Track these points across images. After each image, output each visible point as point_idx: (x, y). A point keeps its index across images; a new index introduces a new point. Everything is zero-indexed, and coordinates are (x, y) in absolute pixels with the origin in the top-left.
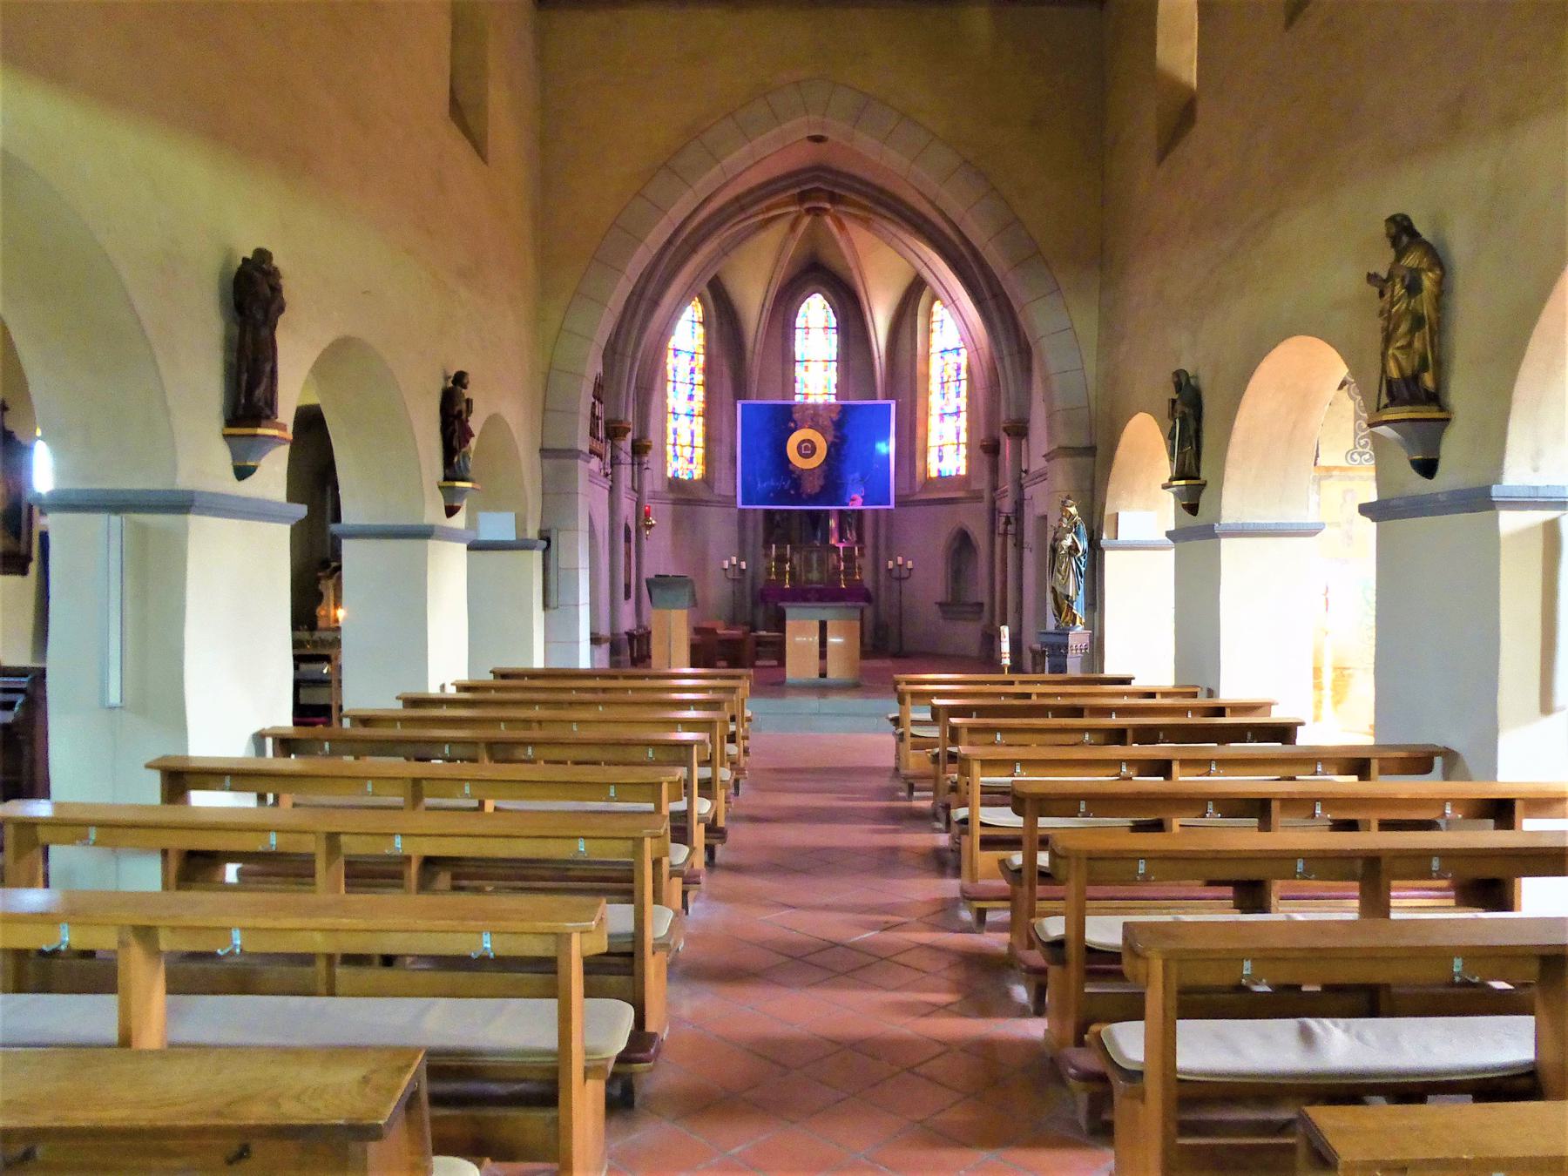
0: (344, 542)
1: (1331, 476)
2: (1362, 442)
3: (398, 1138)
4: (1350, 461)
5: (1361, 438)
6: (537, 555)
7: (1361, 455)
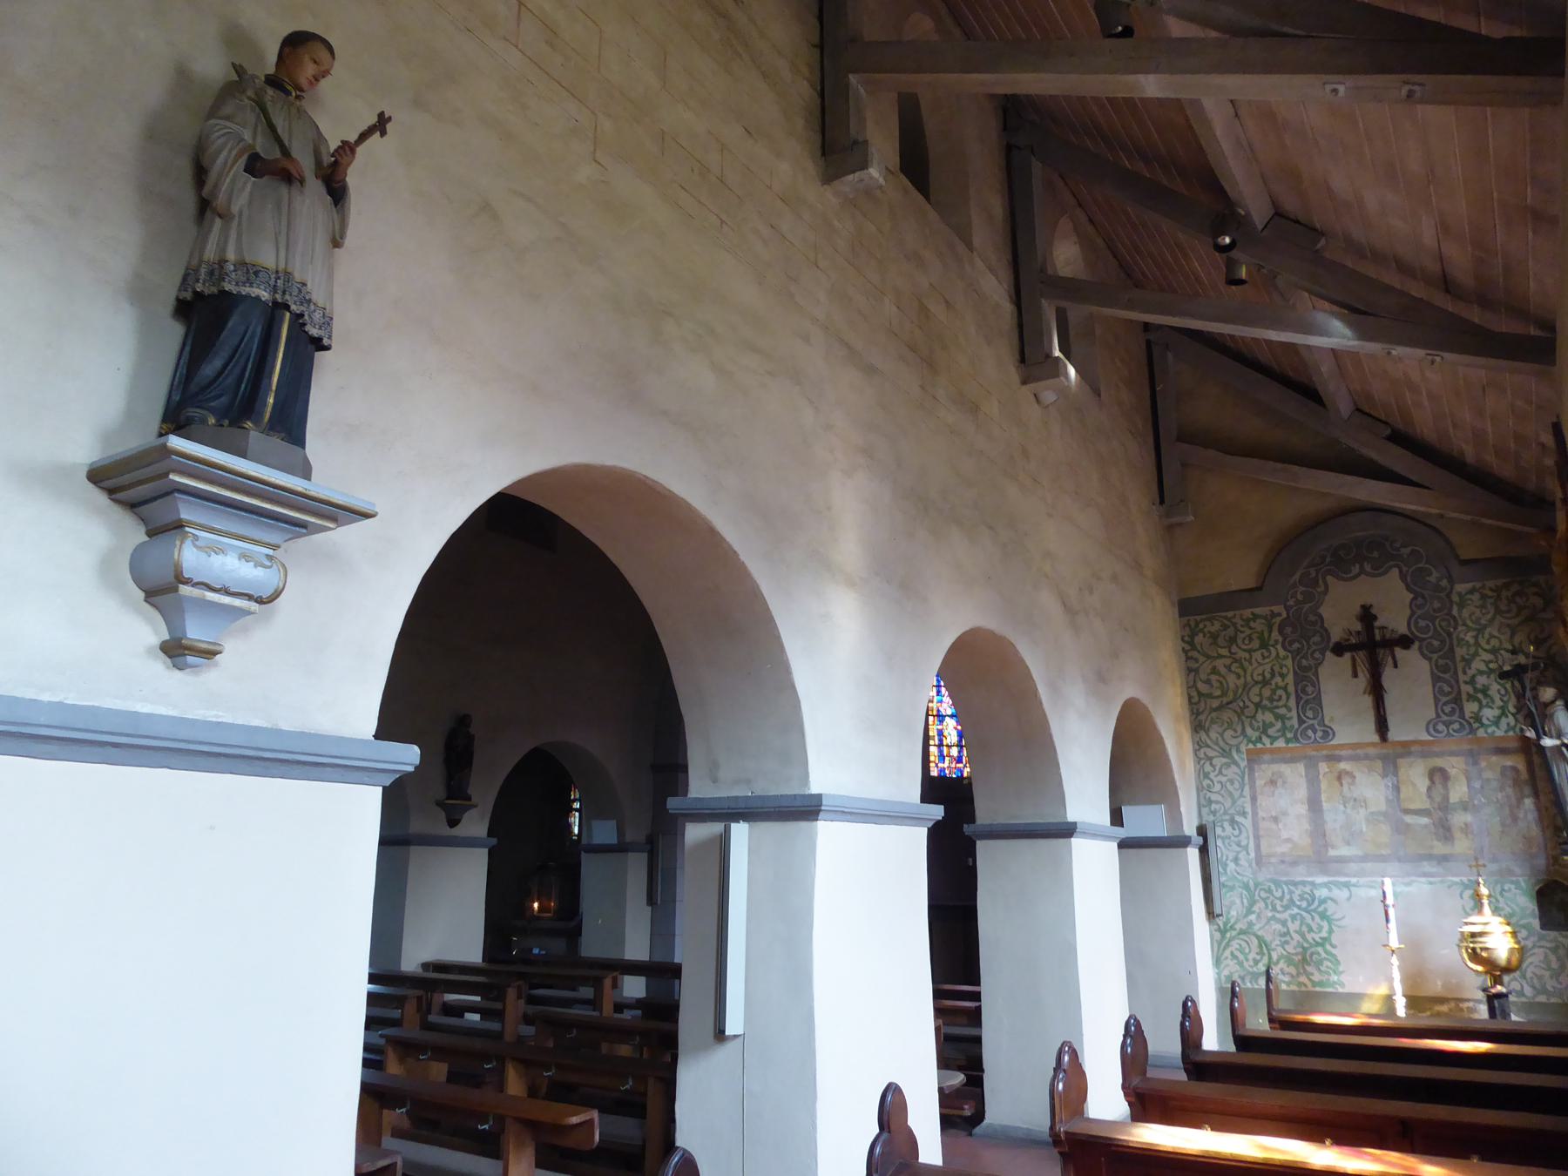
0: (979, 844)
2: (1447, 709)
4: (1433, 732)
5: (1445, 704)
6: (1193, 854)
7: (1447, 724)
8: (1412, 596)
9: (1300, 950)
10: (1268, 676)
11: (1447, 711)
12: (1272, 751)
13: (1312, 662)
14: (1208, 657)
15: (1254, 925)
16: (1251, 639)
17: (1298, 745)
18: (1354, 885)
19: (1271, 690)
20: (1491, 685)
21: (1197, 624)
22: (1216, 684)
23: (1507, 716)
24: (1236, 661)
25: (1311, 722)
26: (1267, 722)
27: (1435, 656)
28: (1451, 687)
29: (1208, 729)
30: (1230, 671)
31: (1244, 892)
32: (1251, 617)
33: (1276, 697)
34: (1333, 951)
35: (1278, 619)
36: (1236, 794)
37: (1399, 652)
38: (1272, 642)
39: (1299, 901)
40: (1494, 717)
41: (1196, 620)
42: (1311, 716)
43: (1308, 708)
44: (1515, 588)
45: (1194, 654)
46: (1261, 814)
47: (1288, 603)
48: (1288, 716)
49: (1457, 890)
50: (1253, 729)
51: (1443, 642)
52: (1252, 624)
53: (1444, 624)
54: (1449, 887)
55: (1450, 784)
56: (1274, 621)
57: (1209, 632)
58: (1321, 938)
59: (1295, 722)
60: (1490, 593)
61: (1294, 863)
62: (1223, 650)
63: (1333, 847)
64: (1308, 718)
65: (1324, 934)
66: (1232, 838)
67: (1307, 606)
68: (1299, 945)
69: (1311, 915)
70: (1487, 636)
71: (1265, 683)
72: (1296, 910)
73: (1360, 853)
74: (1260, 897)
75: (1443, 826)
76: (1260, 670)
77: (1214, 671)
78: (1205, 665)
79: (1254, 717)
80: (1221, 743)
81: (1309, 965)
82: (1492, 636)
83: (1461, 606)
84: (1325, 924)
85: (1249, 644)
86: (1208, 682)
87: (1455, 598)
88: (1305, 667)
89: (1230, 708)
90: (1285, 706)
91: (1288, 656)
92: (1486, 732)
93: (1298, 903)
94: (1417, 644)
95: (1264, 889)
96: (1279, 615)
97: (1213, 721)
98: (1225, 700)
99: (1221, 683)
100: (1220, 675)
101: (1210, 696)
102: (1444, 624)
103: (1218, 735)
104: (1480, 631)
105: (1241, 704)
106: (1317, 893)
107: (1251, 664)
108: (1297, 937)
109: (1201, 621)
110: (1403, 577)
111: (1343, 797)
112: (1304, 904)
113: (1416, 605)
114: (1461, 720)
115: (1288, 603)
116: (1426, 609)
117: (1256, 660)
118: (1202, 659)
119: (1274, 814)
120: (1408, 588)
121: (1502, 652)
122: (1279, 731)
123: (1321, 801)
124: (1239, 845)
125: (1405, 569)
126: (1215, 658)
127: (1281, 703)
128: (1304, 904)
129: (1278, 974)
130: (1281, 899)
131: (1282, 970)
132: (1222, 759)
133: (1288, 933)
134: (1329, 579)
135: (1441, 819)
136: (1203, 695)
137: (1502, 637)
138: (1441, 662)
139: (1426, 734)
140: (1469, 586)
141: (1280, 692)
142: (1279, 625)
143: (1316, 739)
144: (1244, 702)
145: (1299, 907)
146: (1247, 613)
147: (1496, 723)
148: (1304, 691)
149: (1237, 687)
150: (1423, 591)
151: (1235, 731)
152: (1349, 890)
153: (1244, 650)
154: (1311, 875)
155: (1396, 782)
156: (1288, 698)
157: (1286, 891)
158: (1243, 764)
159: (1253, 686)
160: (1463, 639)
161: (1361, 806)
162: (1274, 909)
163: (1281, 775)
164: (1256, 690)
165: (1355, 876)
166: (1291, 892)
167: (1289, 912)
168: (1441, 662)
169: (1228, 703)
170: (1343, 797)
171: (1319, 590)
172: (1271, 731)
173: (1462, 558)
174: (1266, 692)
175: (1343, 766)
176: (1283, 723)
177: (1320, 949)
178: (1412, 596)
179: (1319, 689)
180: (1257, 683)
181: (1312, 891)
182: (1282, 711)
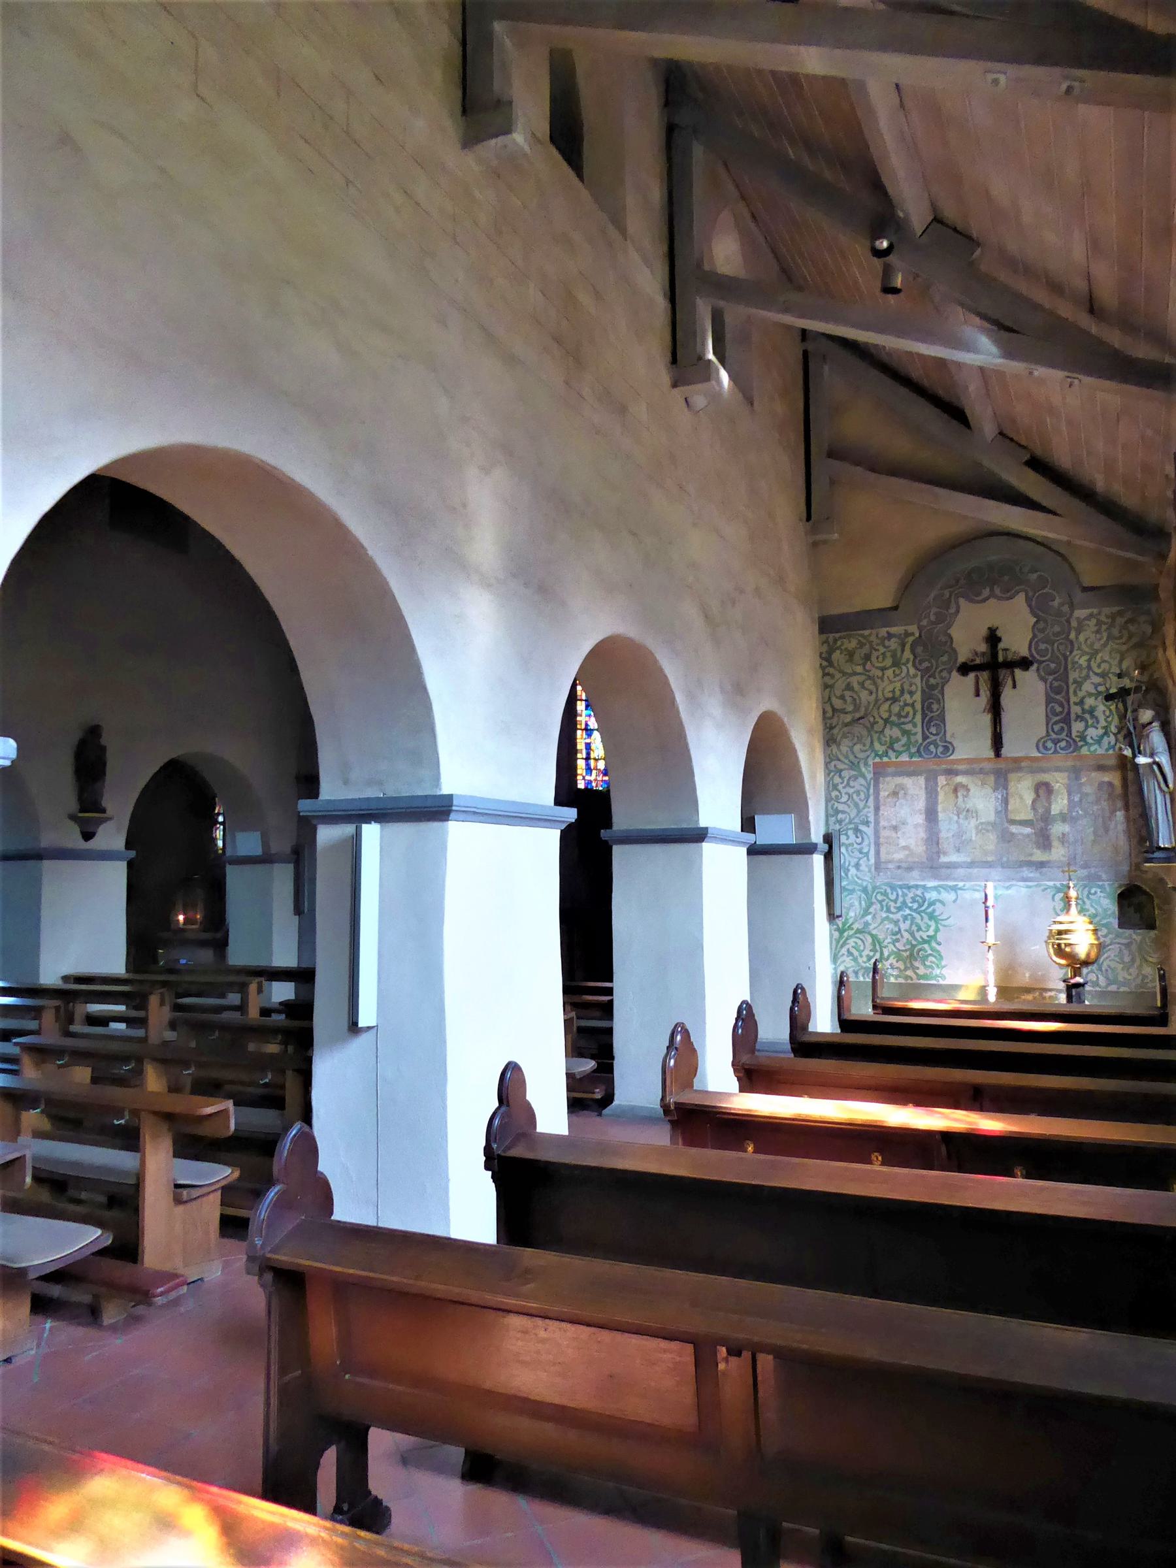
2: (1056, 728)
5: (1056, 723)
6: (818, 860)
7: (1056, 742)
9: (908, 947)
10: (898, 693)
14: (844, 674)
15: (870, 924)
18: (960, 889)
21: (835, 641)
24: (869, 678)
25: (933, 738)
26: (894, 737)
27: (1051, 678)
28: (1063, 708)
34: (937, 947)
35: (911, 639)
36: (861, 805)
39: (911, 903)
45: (831, 670)
46: (883, 823)
47: (921, 624)
49: (1050, 892)
53: (1061, 648)
54: (1044, 890)
58: (928, 936)
59: (919, 737)
61: (910, 869)
63: (945, 854)
64: (931, 733)
65: (931, 933)
66: (855, 846)
69: (922, 916)
71: (894, 700)
72: (908, 912)
76: (890, 688)
77: (849, 687)
78: (840, 682)
79: (882, 732)
80: (851, 757)
84: (932, 923)
86: (842, 697)
87: (1074, 624)
92: (1089, 751)
93: (910, 905)
94: (1035, 666)
96: (913, 634)
97: (844, 736)
98: (858, 715)
99: (855, 700)
105: (872, 719)
106: (927, 896)
107: (883, 681)
108: (906, 935)
110: (1028, 600)
112: (915, 906)
114: (1068, 739)
118: (838, 675)
119: (894, 824)
122: (903, 746)
124: (861, 852)
125: (1030, 594)
128: (915, 906)
130: (895, 901)
134: (962, 601)
138: (1056, 684)
143: (937, 753)
145: (910, 909)
146: (883, 632)
147: (1099, 742)
151: (864, 745)
155: (1005, 795)
156: (914, 714)
157: (900, 893)
158: (869, 776)
162: (888, 910)
163: (902, 787)
164: (886, 706)
165: (962, 880)
167: (901, 913)
168: (1056, 684)
172: (896, 746)
174: (896, 708)
175: (960, 779)
176: (909, 738)
177: (926, 946)
180: (887, 699)
181: (923, 893)
182: (908, 727)
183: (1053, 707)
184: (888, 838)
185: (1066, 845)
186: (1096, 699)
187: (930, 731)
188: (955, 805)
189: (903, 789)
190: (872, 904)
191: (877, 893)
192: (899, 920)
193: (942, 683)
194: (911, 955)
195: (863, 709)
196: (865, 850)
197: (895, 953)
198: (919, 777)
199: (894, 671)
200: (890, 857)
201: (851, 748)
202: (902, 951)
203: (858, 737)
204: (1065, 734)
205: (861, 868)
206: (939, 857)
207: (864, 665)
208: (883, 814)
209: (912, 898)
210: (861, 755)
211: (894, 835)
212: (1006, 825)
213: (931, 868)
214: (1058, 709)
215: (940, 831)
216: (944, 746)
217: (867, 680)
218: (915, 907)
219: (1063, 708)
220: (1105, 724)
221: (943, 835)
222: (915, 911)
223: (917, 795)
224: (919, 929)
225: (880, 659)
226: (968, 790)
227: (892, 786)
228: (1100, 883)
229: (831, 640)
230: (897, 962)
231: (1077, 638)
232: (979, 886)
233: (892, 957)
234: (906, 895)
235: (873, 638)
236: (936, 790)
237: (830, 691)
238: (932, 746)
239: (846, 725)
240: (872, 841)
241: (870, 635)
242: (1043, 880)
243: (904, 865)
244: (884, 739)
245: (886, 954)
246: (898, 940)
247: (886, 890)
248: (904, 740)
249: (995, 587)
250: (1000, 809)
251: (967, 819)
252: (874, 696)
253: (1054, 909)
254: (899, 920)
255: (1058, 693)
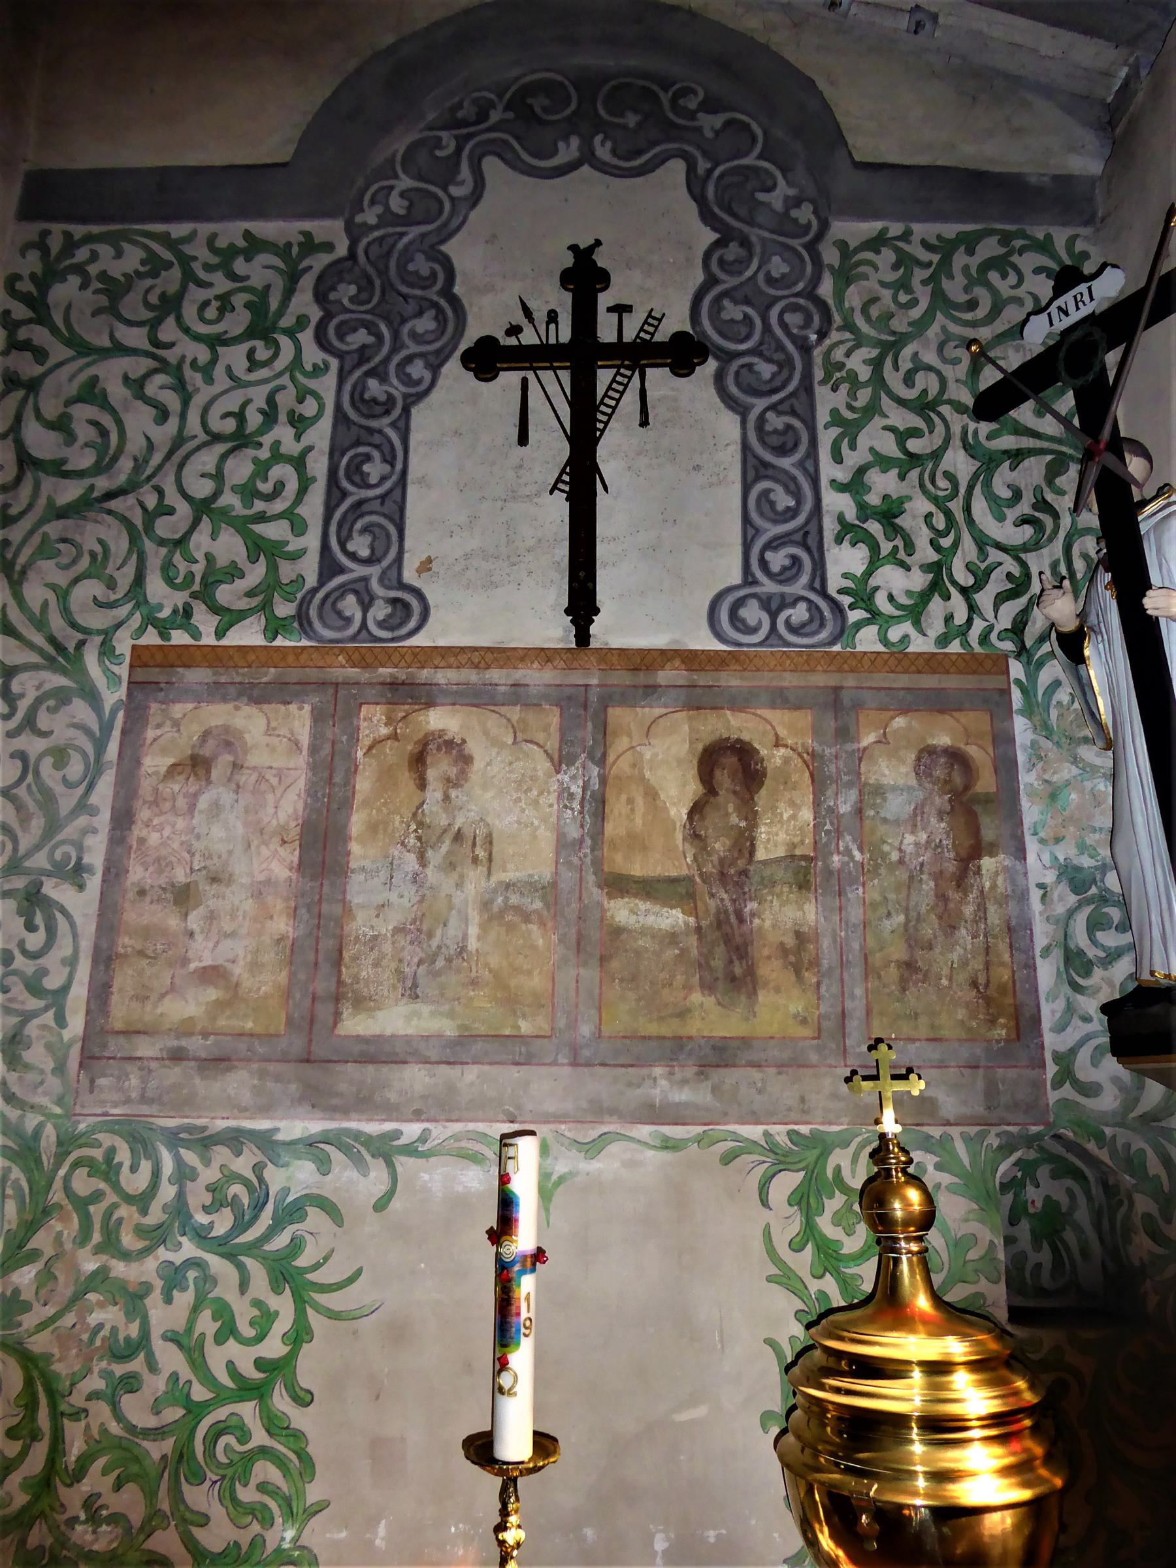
1: (651, 690)
2: (777, 560)
3: (64, 771)
5: (773, 544)
7: (774, 607)
8: (711, 236)
9: (174, 1414)
10: (254, 420)
11: (775, 567)
12: (216, 657)
13: (397, 389)
14: (83, 349)
15: (26, 1307)
16: (225, 304)
17: (305, 643)
18: (410, 1150)
19: (256, 461)
20: (910, 498)
21: (71, 245)
22: (85, 433)
23: (947, 597)
24: (163, 366)
25: (360, 571)
26: (222, 561)
27: (760, 404)
28: (797, 495)
29: (23, 572)
30: (141, 396)
31: (17, 1173)
32: (242, 243)
33: (266, 487)
34: (299, 1418)
35: (320, 261)
36: (67, 802)
37: (658, 378)
38: (287, 322)
39: (206, 1209)
40: (909, 593)
41: (68, 235)
42: (365, 553)
43: (358, 525)
44: (989, 248)
45: (39, 335)
46: (136, 874)
47: (359, 219)
48: (290, 548)
49: (754, 1168)
50: (170, 581)
51: (786, 364)
52: (240, 266)
53: (793, 319)
54: (728, 1159)
55: (762, 798)
56: (305, 263)
57: (103, 276)
58: (260, 1364)
59: (310, 568)
60: (924, 255)
61: (218, 1062)
62: (136, 331)
63: (361, 1003)
64: (353, 556)
65: (273, 1347)
66: (20, 961)
67: (414, 232)
68: (177, 1391)
69: (240, 1267)
70: (906, 365)
71: (241, 440)
72: (189, 1249)
73: (449, 1029)
74: (67, 1188)
75: (727, 940)
76: (232, 403)
77: (92, 393)
78: (65, 372)
79: (180, 543)
80: (57, 623)
81: (198, 1478)
82: (919, 366)
83: (845, 276)
84: (283, 1305)
85: (218, 320)
86: (62, 425)
87: (830, 256)
88: (374, 401)
89: (110, 512)
90: (289, 515)
91: (327, 367)
92: (885, 641)
93: (202, 1218)
94: (711, 365)
95: (88, 1162)
96: (329, 247)
97: (46, 550)
98: (102, 484)
99: (104, 433)
100: (104, 402)
101: (59, 469)
102: (793, 319)
103: (51, 596)
104: (892, 347)
105: (151, 502)
106: (275, 1178)
107: (209, 380)
108: (171, 1359)
109: (89, 239)
110: (695, 186)
111: (420, 824)
112: (222, 1223)
113: (722, 262)
114: (813, 597)
115: (359, 219)
116: (749, 273)
117: (229, 369)
118: (59, 352)
119: (180, 876)
120: (707, 216)
121: (945, 409)
122: (250, 594)
123: (345, 838)
124: (34, 987)
125: (703, 165)
126: (104, 353)
127: (279, 506)
128: (222, 1223)
129: (74, 1520)
130: (142, 1201)
131: (90, 1503)
132: (45, 675)
133: (143, 1343)
134: (492, 166)
135: (721, 914)
136: (37, 464)
137: (948, 371)
138: (775, 422)
139: (705, 631)
140: (870, 228)
141: (283, 472)
142: (320, 278)
143: (364, 624)
144: (161, 493)
145: (201, 1236)
146: (231, 232)
147: (915, 612)
148: (356, 473)
149: (151, 447)
150: (746, 229)
151: (111, 585)
152: (390, 1165)
153: (197, 338)
154: (265, 1110)
155: (595, 784)
156: (302, 491)
157: (168, 1166)
158: (113, 696)
159: (204, 445)
160: (840, 366)
161: (475, 860)
162: (110, 1245)
163: (229, 740)
164: (207, 460)
165: (418, 1116)
166: (184, 1174)
167: (163, 1254)
168: (775, 422)
169: (110, 495)
170: (420, 824)
171: (455, 191)
172: (225, 594)
173: (857, 158)
174: (240, 469)
175: (438, 719)
176: (273, 568)
177: (248, 1410)
178: (711, 236)
179: (404, 472)
180: (216, 438)
181: (258, 1169)
182: (274, 531)
183: (766, 493)
184: (147, 932)
185: (810, 978)
186: (902, 477)
187: (351, 547)
188: (415, 815)
189: (228, 744)
190: (46, 1212)
191: (76, 1165)
192: (147, 1288)
193: (406, 396)
194: (183, 1455)
195: (125, 465)
196: (52, 982)
197: (119, 1444)
198: (293, 707)
199: (251, 354)
200: (148, 1013)
201: (63, 595)
202: (147, 1433)
203: (93, 555)
204: (804, 579)
205: (28, 1056)
206: (337, 1016)
207: (154, 325)
208: (142, 841)
209: (212, 1189)
210: (97, 620)
211: (173, 922)
212: (596, 893)
213: (307, 1060)
214: (784, 501)
215: (348, 911)
216: (394, 601)
217: (155, 371)
218: (220, 1230)
219: (797, 495)
220: (932, 556)
221: (361, 924)
222: (227, 1249)
223: (280, 775)
224: (228, 1331)
225: (211, 313)
226: (466, 760)
227: (187, 739)
228: (936, 1132)
229: (55, 244)
230: (118, 1486)
231: (839, 295)
232: (483, 1137)
233: (101, 1462)
234: (193, 1175)
235: (199, 251)
236: (349, 756)
237: (24, 401)
238: (351, 599)
239: (62, 513)
240: (86, 946)
241: (191, 238)
242: (724, 1118)
243: (196, 1045)
244: (182, 566)
245: (76, 1448)
246: (130, 1383)
247: (112, 1151)
248: (256, 573)
249: (598, 139)
250: (574, 833)
251: (452, 866)
252: (173, 424)
253: (767, 1233)
254: (147, 1288)
255: (782, 450)
